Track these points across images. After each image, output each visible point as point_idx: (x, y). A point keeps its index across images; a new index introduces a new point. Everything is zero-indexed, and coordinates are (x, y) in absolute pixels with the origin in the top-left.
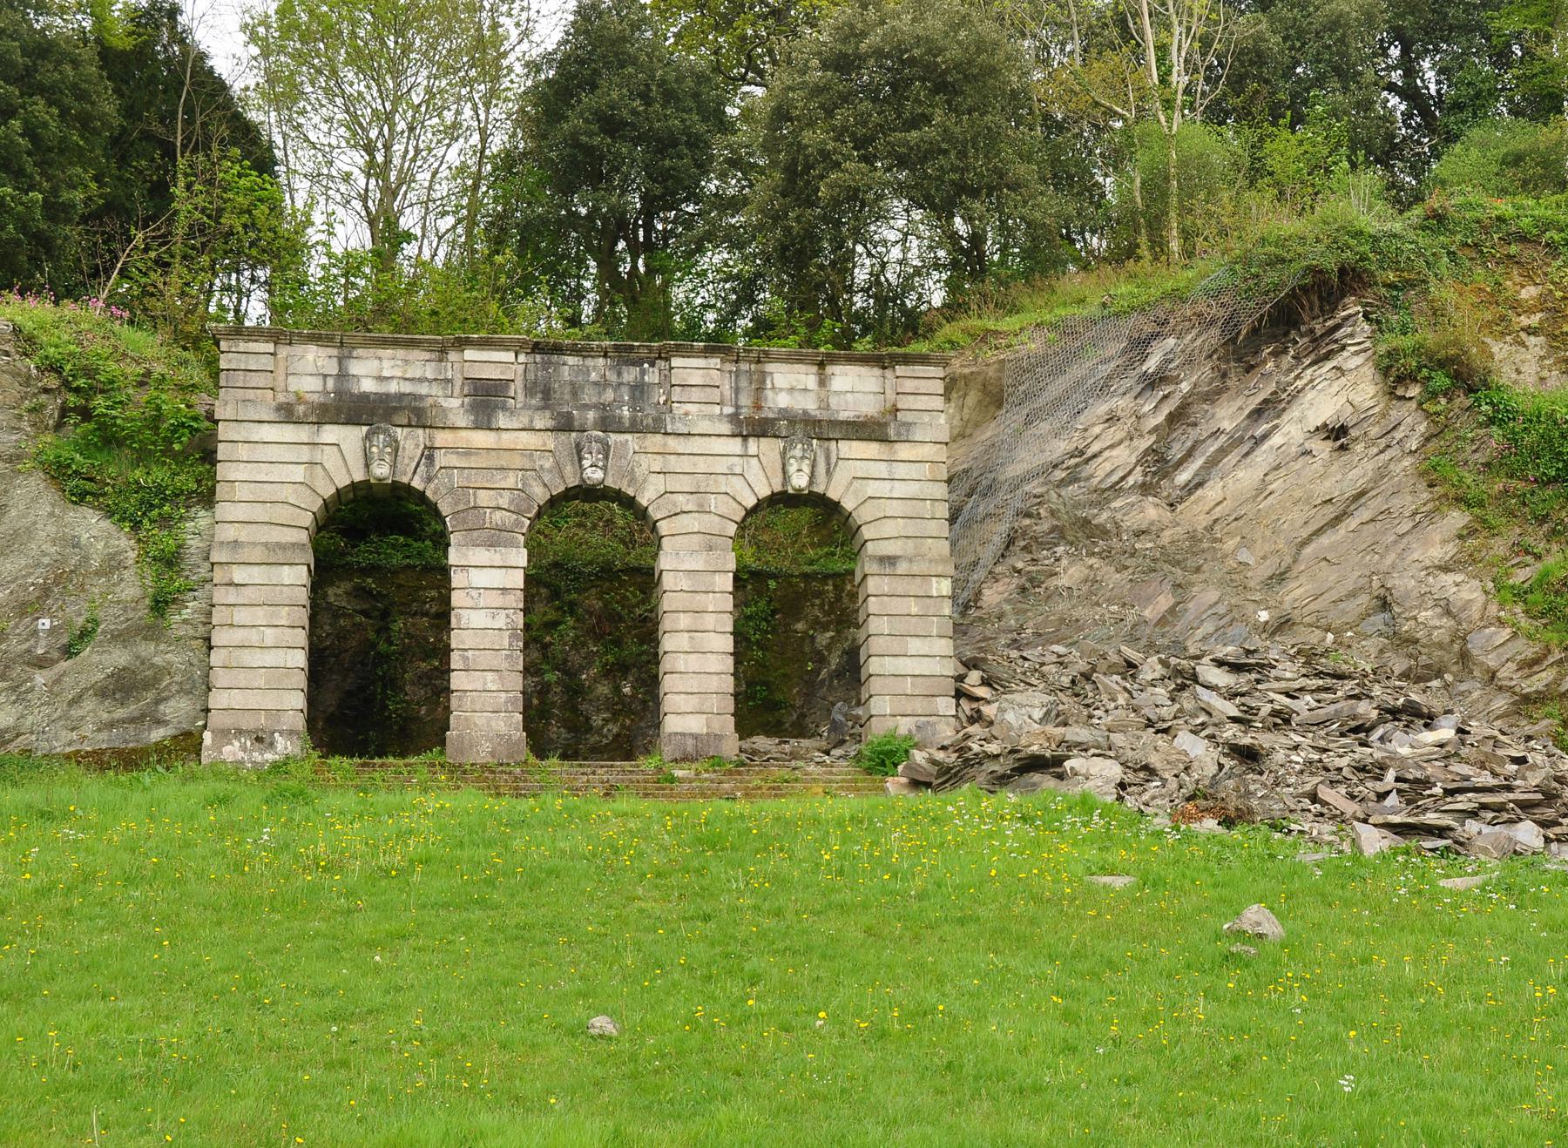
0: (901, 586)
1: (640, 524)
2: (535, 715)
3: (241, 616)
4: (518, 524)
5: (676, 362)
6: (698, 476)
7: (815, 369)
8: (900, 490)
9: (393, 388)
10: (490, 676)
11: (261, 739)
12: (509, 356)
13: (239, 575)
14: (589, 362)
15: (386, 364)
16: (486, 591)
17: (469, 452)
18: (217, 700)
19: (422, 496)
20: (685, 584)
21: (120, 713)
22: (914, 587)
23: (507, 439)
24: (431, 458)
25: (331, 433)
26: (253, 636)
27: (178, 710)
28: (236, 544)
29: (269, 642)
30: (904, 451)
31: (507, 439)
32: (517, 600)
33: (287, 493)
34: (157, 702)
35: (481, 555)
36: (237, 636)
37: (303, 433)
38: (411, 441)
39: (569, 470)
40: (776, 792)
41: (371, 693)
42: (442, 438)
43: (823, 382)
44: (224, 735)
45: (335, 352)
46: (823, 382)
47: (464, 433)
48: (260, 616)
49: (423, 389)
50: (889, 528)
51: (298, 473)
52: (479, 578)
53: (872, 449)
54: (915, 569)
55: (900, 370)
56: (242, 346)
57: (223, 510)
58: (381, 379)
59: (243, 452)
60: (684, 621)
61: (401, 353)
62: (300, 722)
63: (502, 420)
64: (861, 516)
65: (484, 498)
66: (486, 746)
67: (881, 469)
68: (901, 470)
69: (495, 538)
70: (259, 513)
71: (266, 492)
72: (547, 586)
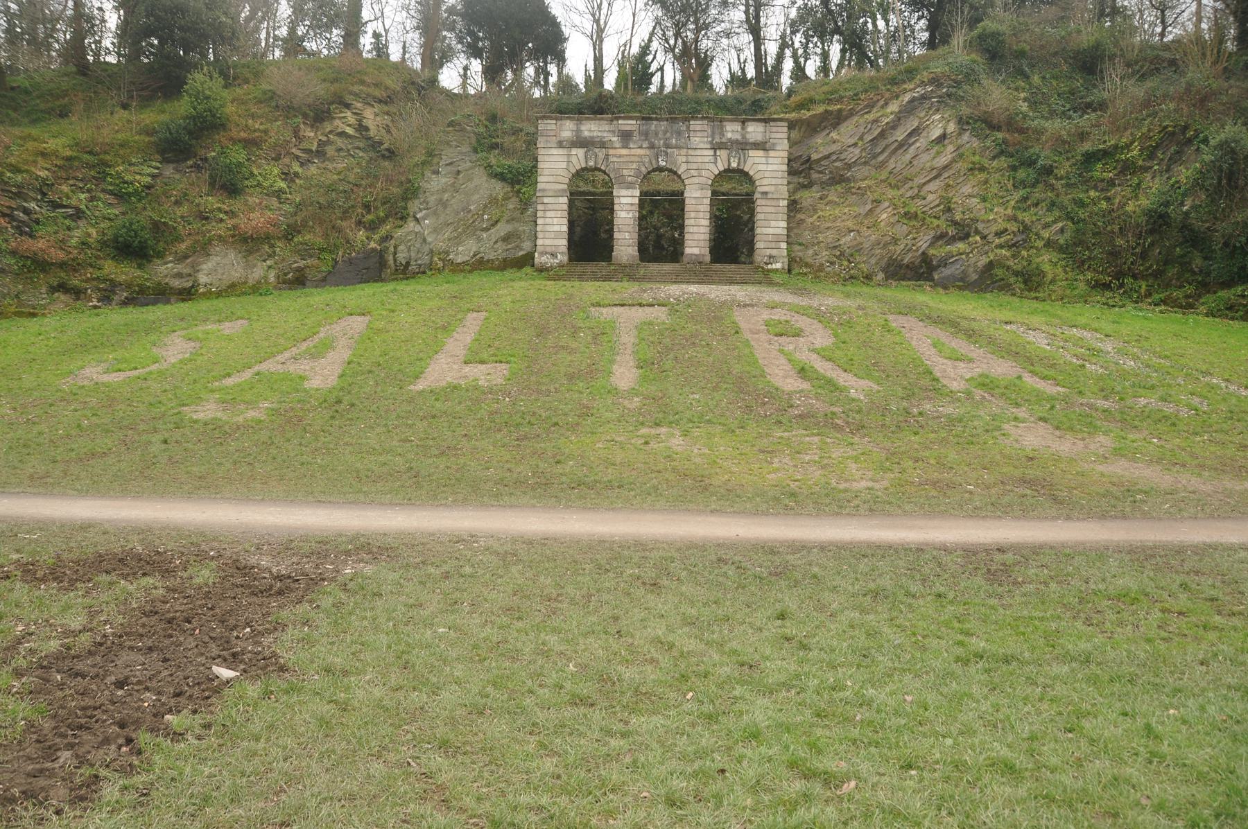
0: (769, 203)
11: (553, 255)
13: (546, 200)
16: (626, 204)
17: (620, 156)
18: (539, 242)
22: (774, 203)
23: (633, 152)
25: (574, 151)
27: (527, 246)
30: (772, 153)
38: (601, 153)
42: (611, 152)
43: (743, 129)
44: (542, 254)
50: (765, 182)
52: (624, 200)
53: (761, 153)
59: (546, 158)
60: (693, 215)
62: (565, 249)
64: (756, 177)
65: (625, 172)
69: (630, 186)
71: (554, 172)
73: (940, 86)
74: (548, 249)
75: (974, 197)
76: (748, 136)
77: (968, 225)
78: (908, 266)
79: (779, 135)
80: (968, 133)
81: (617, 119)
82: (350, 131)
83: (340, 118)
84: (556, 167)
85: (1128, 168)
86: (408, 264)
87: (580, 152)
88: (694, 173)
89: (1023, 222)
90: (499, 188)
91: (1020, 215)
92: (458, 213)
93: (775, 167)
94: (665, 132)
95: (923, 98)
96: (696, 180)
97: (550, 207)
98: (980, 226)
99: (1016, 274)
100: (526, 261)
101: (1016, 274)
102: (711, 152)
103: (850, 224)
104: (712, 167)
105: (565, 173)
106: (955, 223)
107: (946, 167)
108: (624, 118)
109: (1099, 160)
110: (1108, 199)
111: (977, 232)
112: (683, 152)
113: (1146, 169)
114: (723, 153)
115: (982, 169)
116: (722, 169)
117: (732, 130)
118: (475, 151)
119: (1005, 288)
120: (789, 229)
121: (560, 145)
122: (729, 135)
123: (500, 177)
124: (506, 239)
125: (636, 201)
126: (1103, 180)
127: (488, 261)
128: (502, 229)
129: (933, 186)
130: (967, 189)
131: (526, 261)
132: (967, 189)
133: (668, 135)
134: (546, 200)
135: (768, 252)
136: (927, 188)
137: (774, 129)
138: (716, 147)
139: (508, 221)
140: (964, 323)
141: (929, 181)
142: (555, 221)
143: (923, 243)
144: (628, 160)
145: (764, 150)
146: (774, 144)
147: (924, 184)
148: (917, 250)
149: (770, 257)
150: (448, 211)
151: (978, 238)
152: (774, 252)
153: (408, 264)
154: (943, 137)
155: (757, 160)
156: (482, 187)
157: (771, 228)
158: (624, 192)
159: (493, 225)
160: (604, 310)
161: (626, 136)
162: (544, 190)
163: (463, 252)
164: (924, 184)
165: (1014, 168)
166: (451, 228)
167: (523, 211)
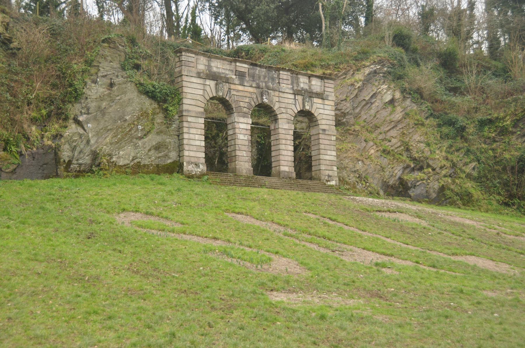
2: (209, 160)
4: (249, 112)
5: (281, 72)
7: (308, 78)
9: (220, 71)
10: (244, 152)
11: (197, 165)
12: (246, 66)
13: (190, 119)
14: (262, 70)
15: (219, 64)
16: (242, 128)
17: (238, 91)
19: (228, 101)
20: (283, 132)
21: (160, 155)
23: (246, 89)
24: (230, 92)
25: (208, 82)
27: (173, 155)
29: (196, 139)
30: (326, 102)
31: (246, 89)
32: (249, 132)
33: (199, 97)
34: (168, 152)
38: (226, 86)
39: (259, 99)
42: (233, 87)
43: (310, 82)
44: (189, 163)
45: (207, 58)
46: (310, 82)
47: (237, 86)
49: (227, 72)
50: (324, 122)
51: (201, 92)
53: (320, 101)
54: (329, 133)
55: (326, 81)
56: (188, 54)
58: (217, 67)
59: (188, 84)
60: (284, 142)
61: (222, 61)
62: (203, 161)
64: (319, 118)
65: (242, 104)
66: (244, 171)
69: (245, 115)
71: (194, 97)
73: (383, 66)
74: (193, 160)
75: (422, 142)
76: (312, 88)
77: (422, 161)
78: (392, 186)
79: (330, 90)
80: (409, 100)
81: (235, 61)
84: (195, 93)
85: (503, 132)
86: (70, 162)
87: (212, 83)
88: (283, 110)
89: (452, 161)
90: (148, 104)
91: (449, 156)
92: (115, 121)
93: (327, 112)
94: (265, 77)
95: (375, 72)
97: (192, 125)
98: (431, 163)
99: (457, 194)
100: (176, 168)
101: (457, 194)
102: (292, 96)
103: (356, 155)
104: (293, 107)
105: (201, 98)
106: (414, 159)
107: (399, 122)
108: (241, 62)
109: (486, 125)
110: (493, 150)
111: (429, 166)
112: (277, 93)
113: (513, 133)
114: (299, 98)
115: (423, 125)
116: (299, 110)
117: (303, 81)
118: (123, 68)
119: (453, 204)
120: (338, 156)
121: (199, 75)
122: (302, 85)
123: (151, 95)
124: (157, 148)
125: (249, 127)
126: (489, 138)
127: (144, 166)
128: (153, 139)
129: (394, 133)
130: (417, 137)
131: (176, 168)
132: (417, 137)
133: (266, 79)
134: (190, 119)
135: (327, 172)
136: (389, 134)
138: (296, 93)
139: (158, 133)
140: (281, 222)
141: (390, 130)
142: (197, 137)
143: (398, 172)
145: (323, 99)
146: (327, 96)
147: (388, 131)
148: (395, 176)
149: (329, 176)
150: (107, 118)
151: (430, 170)
152: (331, 173)
153: (70, 162)
154: (392, 101)
156: (135, 102)
157: (327, 156)
158: (242, 120)
159: (145, 135)
161: (241, 75)
162: (188, 111)
163: (124, 156)
164: (388, 131)
165: (439, 126)
166: (111, 135)
167: (169, 126)
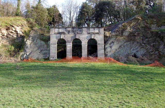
0: (100, 46)
1: (80, 42)
3: (52, 49)
6: (84, 38)
8: (100, 38)
9: (62, 31)
13: (52, 46)
16: (69, 46)
18: (50, 55)
20: (84, 46)
21: (44, 56)
22: (101, 46)
23: (70, 35)
25: (58, 35)
26: (53, 50)
28: (52, 43)
30: (100, 35)
35: (69, 44)
36: (52, 50)
37: (56, 35)
40: (65, 64)
41: (62, 55)
44: (51, 57)
48: (53, 49)
50: (99, 41)
52: (69, 46)
57: (51, 41)
59: (52, 37)
60: (83, 49)
63: (70, 33)
67: (99, 37)
68: (100, 37)
69: (70, 42)
70: (53, 41)
72: (74, 46)
79: (102, 31)
82: (14, 32)
83: (11, 29)
90: (43, 43)
96: (84, 41)
137: (101, 30)
144: (68, 37)
155: (97, 36)
157: (100, 51)
160: (41, 75)
